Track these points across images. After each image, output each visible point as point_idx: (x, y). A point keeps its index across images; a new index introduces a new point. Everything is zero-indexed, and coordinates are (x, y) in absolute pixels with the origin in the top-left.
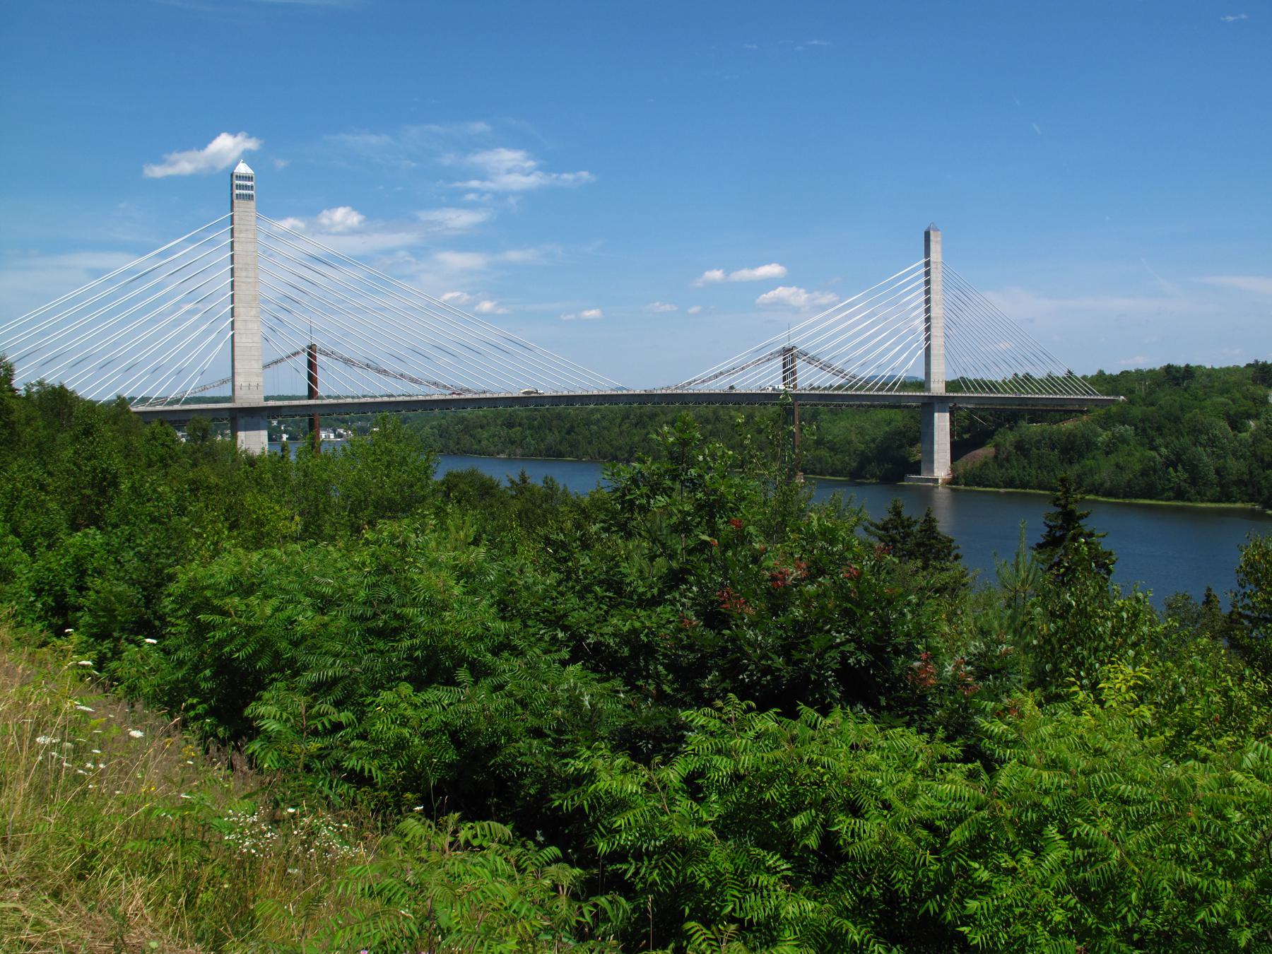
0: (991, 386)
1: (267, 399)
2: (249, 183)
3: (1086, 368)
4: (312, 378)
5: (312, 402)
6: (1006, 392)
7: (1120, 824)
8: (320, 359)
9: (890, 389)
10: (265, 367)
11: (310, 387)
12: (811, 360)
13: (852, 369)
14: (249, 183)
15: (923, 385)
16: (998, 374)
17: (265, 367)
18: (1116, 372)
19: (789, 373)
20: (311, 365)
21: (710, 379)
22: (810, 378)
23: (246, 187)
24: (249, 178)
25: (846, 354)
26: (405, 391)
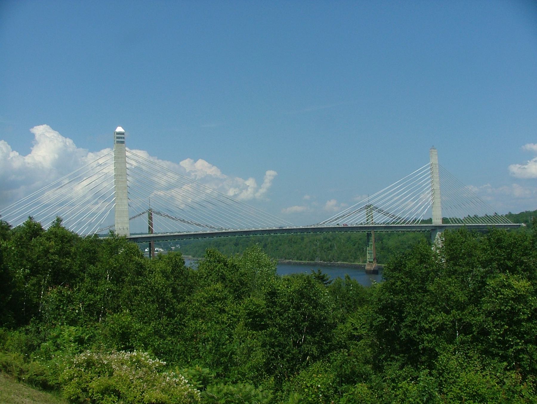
0: (459, 221)
1: (131, 234)
2: (118, 136)
3: (503, 211)
4: (151, 224)
5: (152, 235)
6: (459, 223)
7: (516, 291)
8: (154, 216)
9: (407, 223)
10: (130, 219)
11: (149, 228)
12: (380, 211)
13: (398, 215)
14: (118, 136)
15: (430, 221)
16: (461, 216)
17: (130, 219)
18: (517, 213)
19: (369, 216)
20: (151, 218)
21: (333, 221)
22: (379, 219)
23: (121, 138)
24: (123, 134)
25: (402, 209)
26: (186, 229)
